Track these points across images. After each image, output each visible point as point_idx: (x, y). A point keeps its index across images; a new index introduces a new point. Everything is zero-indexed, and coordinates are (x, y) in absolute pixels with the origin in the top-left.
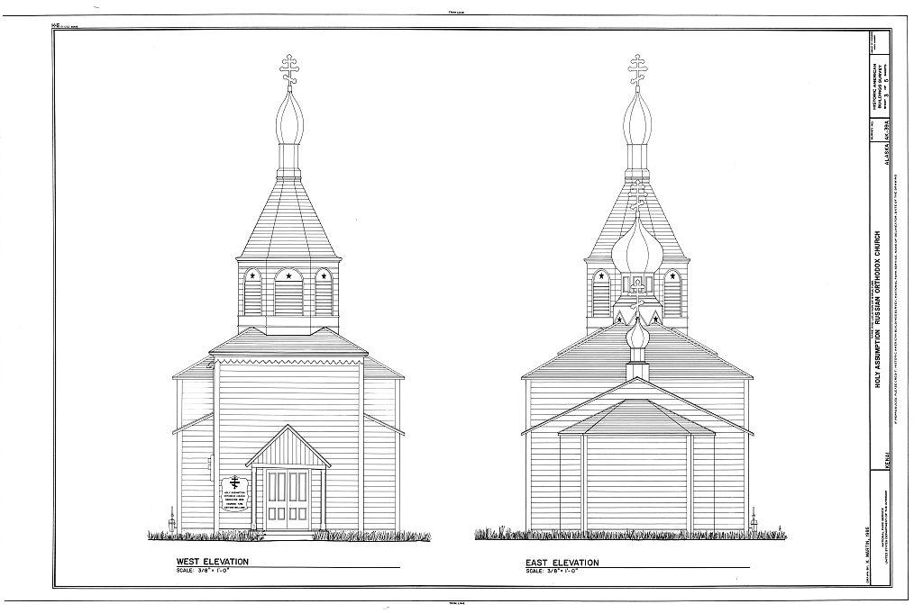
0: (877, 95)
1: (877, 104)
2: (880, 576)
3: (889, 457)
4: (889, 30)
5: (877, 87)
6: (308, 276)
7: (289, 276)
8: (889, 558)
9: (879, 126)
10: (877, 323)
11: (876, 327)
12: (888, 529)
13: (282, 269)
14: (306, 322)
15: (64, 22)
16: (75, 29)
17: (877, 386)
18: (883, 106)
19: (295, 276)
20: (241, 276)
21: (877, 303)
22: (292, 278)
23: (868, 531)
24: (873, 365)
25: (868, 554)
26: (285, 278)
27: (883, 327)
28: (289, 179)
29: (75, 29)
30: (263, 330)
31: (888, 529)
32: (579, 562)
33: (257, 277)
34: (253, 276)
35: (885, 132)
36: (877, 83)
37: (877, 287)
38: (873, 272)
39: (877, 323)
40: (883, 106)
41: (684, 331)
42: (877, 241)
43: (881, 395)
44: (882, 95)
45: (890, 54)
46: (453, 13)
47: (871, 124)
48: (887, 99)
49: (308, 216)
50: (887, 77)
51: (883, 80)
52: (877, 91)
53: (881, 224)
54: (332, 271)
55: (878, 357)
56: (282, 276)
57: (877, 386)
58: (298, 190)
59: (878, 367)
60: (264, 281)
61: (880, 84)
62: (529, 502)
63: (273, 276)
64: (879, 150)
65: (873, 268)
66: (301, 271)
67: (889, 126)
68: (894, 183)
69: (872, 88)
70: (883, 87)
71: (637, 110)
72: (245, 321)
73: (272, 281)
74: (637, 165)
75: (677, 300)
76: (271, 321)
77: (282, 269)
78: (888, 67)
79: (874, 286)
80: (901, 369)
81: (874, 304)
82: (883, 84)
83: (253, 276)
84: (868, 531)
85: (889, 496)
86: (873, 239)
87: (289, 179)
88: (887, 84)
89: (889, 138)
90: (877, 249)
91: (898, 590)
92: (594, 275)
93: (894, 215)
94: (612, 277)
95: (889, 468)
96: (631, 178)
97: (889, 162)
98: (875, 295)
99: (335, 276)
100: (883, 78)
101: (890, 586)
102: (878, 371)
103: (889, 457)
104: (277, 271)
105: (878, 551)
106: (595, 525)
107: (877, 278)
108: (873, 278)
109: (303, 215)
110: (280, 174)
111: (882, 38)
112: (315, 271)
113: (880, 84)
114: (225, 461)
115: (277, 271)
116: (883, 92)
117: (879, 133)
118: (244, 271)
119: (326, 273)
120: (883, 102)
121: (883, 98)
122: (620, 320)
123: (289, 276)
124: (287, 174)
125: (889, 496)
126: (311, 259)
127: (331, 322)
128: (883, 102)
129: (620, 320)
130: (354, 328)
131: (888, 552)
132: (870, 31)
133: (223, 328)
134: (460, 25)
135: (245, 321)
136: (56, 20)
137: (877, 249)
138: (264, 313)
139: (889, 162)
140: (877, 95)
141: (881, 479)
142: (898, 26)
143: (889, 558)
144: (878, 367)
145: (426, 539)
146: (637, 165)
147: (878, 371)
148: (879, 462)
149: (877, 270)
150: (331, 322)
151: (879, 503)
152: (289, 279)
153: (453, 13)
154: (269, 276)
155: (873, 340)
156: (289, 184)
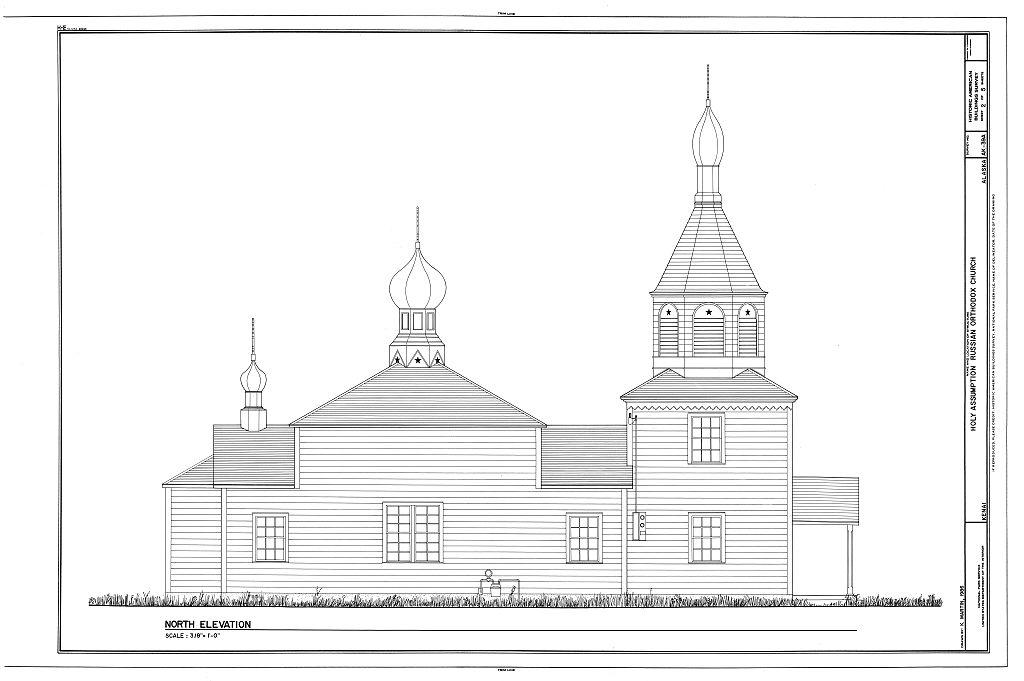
0: (973, 105)
1: (973, 116)
2: (976, 640)
3: (986, 508)
4: (986, 34)
5: (973, 97)
6: (730, 312)
7: (709, 312)
8: (986, 622)
9: (975, 141)
10: (973, 358)
11: (971, 363)
12: (985, 588)
13: (701, 304)
14: (727, 362)
15: (71, 24)
16: (83, 31)
17: (973, 429)
18: (979, 117)
19: (716, 313)
20: (656, 313)
21: (974, 337)
22: (713, 315)
23: (963, 590)
24: (968, 406)
25: (963, 615)
26: (705, 315)
27: (980, 362)
28: (708, 204)
29: (83, 31)
30: (681, 372)
31: (985, 588)
32: (230, 624)
33: (674, 314)
34: (669, 312)
35: (982, 147)
36: (973, 93)
37: (973, 319)
38: (968, 302)
39: (973, 358)
40: (979, 117)
41: (761, 371)
42: (973, 268)
43: (977, 439)
44: (979, 104)
45: (987, 61)
46: (502, 15)
47: (966, 138)
48: (984, 109)
49: (728, 239)
50: (985, 86)
51: (979, 89)
52: (973, 101)
53: (978, 249)
54: (758, 307)
55: (973, 398)
56: (701, 313)
57: (973, 429)
58: (717, 213)
59: (974, 408)
60: (681, 318)
61: (976, 92)
62: (171, 565)
63: (691, 313)
64: (975, 166)
65: (968, 298)
66: (723, 307)
67: (986, 140)
68: (991, 204)
69: (968, 98)
70: (979, 97)
71: (708, 129)
72: (662, 363)
73: (689, 319)
74: (707, 188)
75: (754, 340)
76: (690, 362)
77: (701, 304)
78: (985, 75)
79: (969, 318)
80: (999, 411)
81: (969, 340)
82: (980, 93)
83: (669, 312)
84: (963, 590)
85: (986, 551)
86: (968, 266)
87: (708, 204)
88: (984, 93)
89: (986, 157)
90: (973, 277)
91: (996, 656)
92: (661, 310)
93: (992, 239)
94: (681, 313)
95: (986, 519)
96: (702, 203)
97: (986, 181)
98: (971, 328)
99: (761, 313)
100: (980, 86)
101: (987, 651)
102: (974, 412)
103: (986, 508)
104: (694, 307)
105: (974, 613)
106: (640, 589)
107: (973, 309)
108: (969, 310)
109: (720, 248)
110: (699, 199)
111: (978, 43)
112: (738, 307)
113: (976, 92)
114: (215, 530)
115: (694, 307)
116: (980, 102)
117: (976, 148)
118: (658, 307)
119: (750, 308)
120: (979, 114)
121: (980, 109)
122: (397, 360)
123: (709, 312)
124: (706, 199)
125: (986, 551)
126: (732, 294)
127: (756, 363)
128: (979, 114)
129: (397, 360)
130: (779, 368)
131: (985, 613)
132: (966, 34)
133: (639, 372)
134: (511, 27)
135: (662, 363)
136: (62, 22)
137: (973, 277)
138: (681, 354)
139: (986, 181)
140: (973, 105)
141: (977, 533)
142: (996, 29)
143: (986, 622)
144: (974, 408)
145: (93, 603)
146: (707, 188)
147: (974, 412)
148: (975, 513)
149: (973, 300)
150: (756, 363)
151: (975, 559)
152: (709, 316)
153: (502, 15)
154: (687, 313)
155: (968, 378)
156: (708, 213)
